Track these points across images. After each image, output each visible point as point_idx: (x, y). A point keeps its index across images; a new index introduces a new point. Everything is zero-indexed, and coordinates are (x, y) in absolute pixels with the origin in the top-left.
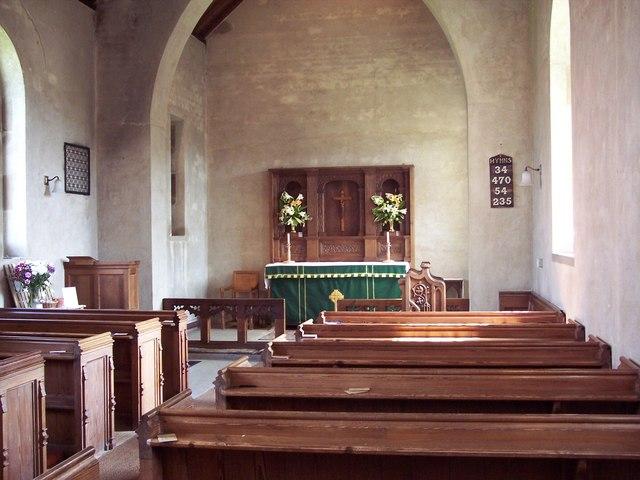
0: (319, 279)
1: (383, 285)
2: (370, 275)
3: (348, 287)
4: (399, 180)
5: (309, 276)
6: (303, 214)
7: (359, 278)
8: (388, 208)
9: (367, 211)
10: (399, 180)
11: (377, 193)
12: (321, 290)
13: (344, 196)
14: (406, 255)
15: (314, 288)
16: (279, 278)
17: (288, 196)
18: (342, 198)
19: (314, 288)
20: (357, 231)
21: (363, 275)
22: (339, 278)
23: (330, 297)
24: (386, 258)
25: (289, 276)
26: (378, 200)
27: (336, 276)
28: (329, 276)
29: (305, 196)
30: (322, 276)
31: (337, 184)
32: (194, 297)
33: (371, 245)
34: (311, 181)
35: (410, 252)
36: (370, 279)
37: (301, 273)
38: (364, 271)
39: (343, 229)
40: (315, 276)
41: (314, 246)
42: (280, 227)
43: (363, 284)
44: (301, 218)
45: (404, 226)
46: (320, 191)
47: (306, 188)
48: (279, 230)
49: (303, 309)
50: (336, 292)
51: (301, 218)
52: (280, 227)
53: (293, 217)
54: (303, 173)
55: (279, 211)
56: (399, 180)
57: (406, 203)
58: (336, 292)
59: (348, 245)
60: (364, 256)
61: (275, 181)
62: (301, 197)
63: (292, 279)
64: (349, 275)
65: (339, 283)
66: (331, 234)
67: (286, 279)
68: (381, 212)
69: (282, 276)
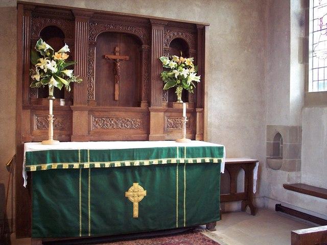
0: (112, 168)
1: (197, 171)
2: (182, 161)
3: (153, 179)
4: (190, 41)
5: (97, 165)
6: (69, 73)
7: (169, 165)
8: (185, 72)
9: (154, 74)
10: (187, 37)
11: (165, 53)
12: (114, 185)
13: (120, 53)
14: (198, 133)
15: (103, 182)
16: (50, 171)
17: (45, 46)
18: (117, 57)
19: (103, 182)
20: (137, 98)
21: (174, 161)
22: (141, 167)
23: (144, 193)
24: (47, 138)
25: (66, 166)
26: (166, 61)
27: (137, 163)
28: (127, 163)
29: (71, 47)
30: (118, 164)
31: (109, 36)
32: (290, 241)
33: (157, 119)
34: (81, 30)
35: (202, 127)
36: (181, 165)
37: (84, 160)
38: (174, 156)
39: (117, 98)
40: (107, 165)
41: (80, 119)
42: (32, 91)
43: (172, 172)
44: (66, 78)
45: (196, 97)
46: (92, 45)
47: (73, 37)
48: (34, 95)
49: (85, 215)
50: (136, 186)
51: (66, 78)
52: (32, 91)
53: (56, 76)
54: (71, 15)
55: (32, 66)
56: (190, 41)
57: (201, 72)
58: (136, 186)
59: (130, 116)
60: (148, 133)
61: (27, 22)
62: (66, 48)
63: (71, 170)
64: (155, 162)
65: (140, 175)
66: (103, 104)
67: (60, 170)
68: (173, 78)
69: (55, 166)
